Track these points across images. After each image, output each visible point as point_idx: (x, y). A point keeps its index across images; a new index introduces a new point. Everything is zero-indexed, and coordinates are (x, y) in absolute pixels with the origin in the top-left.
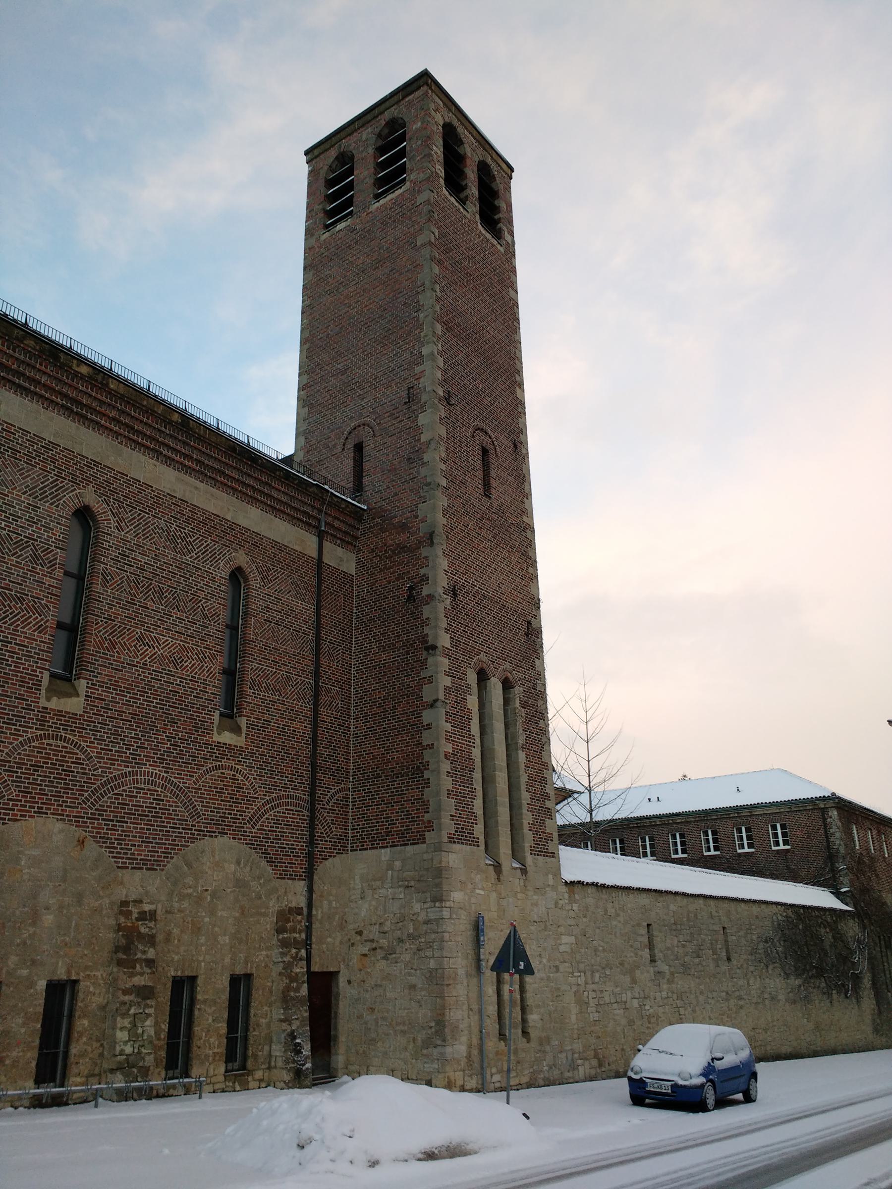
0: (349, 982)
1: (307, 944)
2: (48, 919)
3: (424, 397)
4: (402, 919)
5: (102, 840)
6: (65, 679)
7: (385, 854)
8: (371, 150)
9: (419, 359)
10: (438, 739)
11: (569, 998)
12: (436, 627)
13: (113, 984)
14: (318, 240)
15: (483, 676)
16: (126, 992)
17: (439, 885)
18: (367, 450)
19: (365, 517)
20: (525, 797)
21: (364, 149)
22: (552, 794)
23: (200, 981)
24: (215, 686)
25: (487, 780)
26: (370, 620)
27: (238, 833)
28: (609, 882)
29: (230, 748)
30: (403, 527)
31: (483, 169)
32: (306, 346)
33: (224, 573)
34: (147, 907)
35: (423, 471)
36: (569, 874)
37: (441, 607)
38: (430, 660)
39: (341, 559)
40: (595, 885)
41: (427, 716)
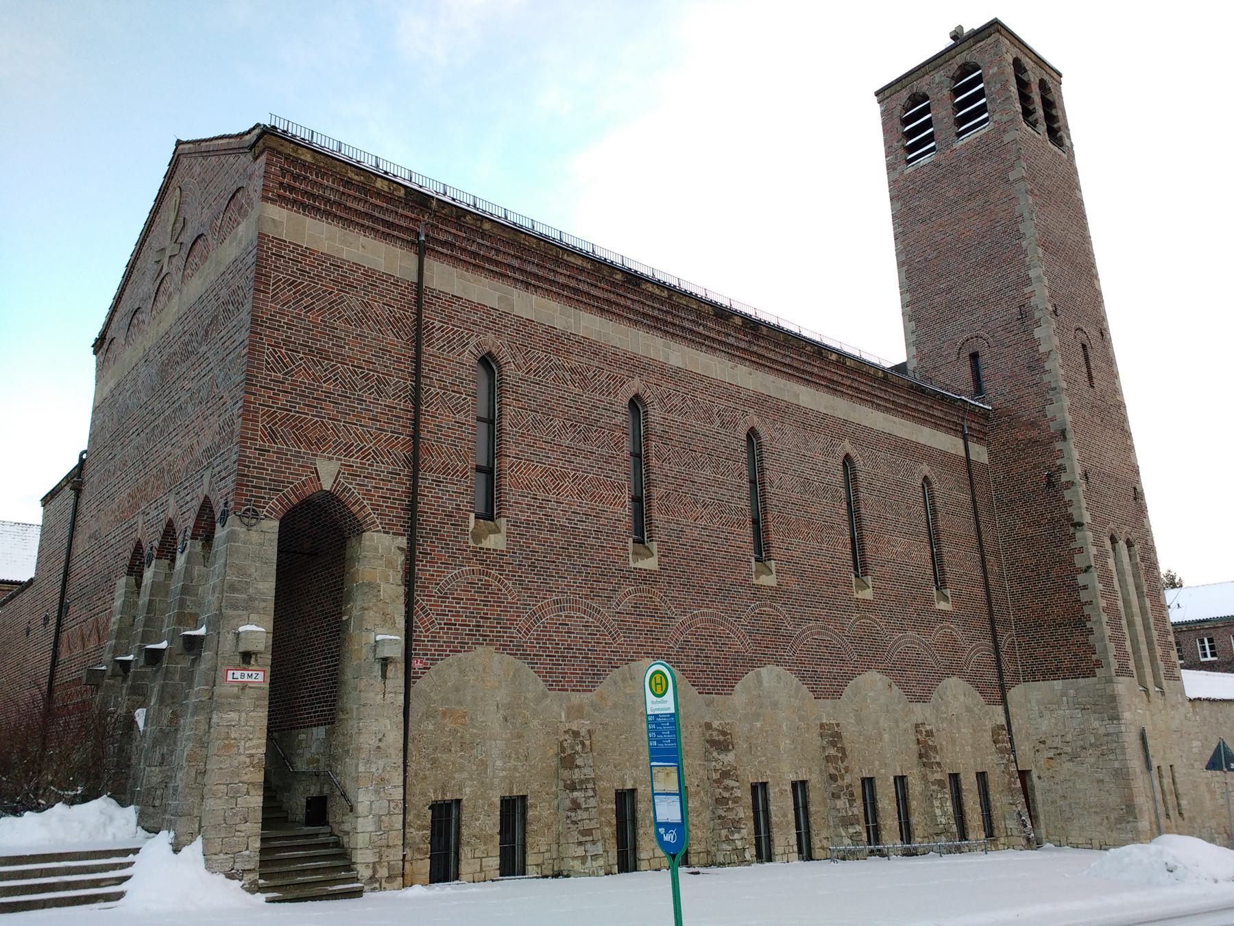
0: (1039, 778)
1: (1013, 750)
2: (886, 737)
3: (1037, 315)
4: (1082, 732)
5: (899, 684)
6: (488, 515)
7: (1058, 685)
8: (946, 92)
9: (1028, 281)
10: (1096, 597)
11: (1203, 788)
12: (1080, 508)
13: (924, 777)
14: (901, 174)
15: (1113, 540)
16: (933, 784)
17: (1115, 708)
18: (983, 360)
19: (991, 415)
20: (1155, 634)
21: (939, 88)
22: (1171, 629)
23: (962, 776)
24: (625, 512)
25: (1131, 624)
26: (1011, 501)
27: (961, 674)
28: (1218, 696)
29: (945, 612)
30: (1033, 425)
31: (1042, 84)
32: (905, 268)
33: (469, 358)
34: (928, 728)
35: (1046, 378)
36: (1191, 693)
37: (1080, 490)
38: (1078, 535)
39: (980, 453)
40: (1208, 700)
41: (1082, 579)
